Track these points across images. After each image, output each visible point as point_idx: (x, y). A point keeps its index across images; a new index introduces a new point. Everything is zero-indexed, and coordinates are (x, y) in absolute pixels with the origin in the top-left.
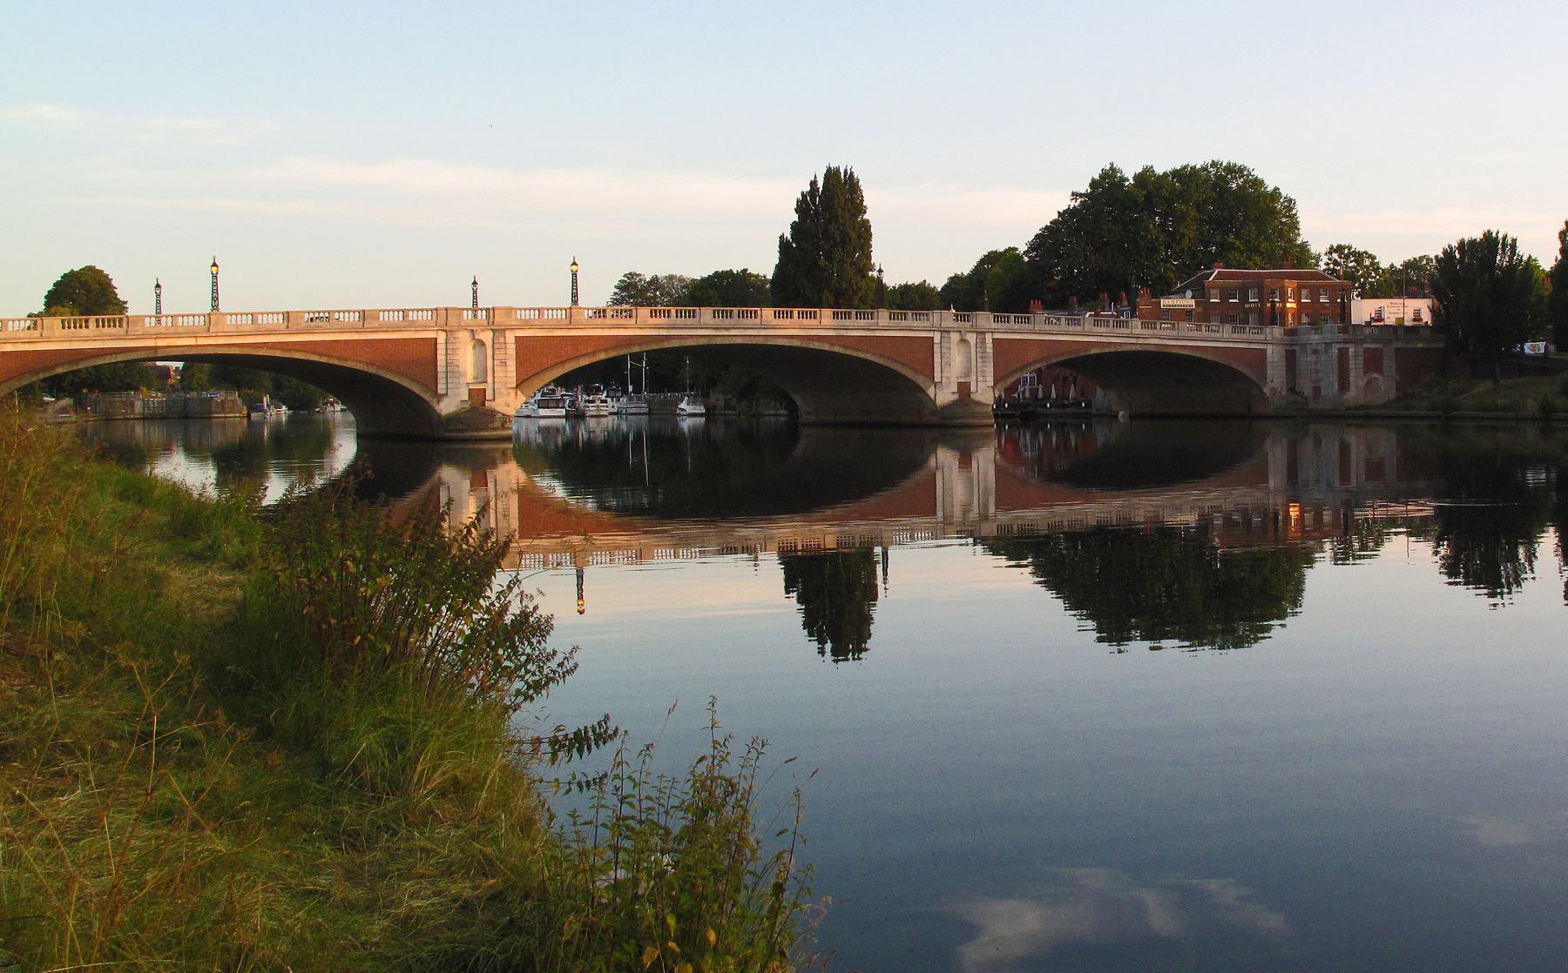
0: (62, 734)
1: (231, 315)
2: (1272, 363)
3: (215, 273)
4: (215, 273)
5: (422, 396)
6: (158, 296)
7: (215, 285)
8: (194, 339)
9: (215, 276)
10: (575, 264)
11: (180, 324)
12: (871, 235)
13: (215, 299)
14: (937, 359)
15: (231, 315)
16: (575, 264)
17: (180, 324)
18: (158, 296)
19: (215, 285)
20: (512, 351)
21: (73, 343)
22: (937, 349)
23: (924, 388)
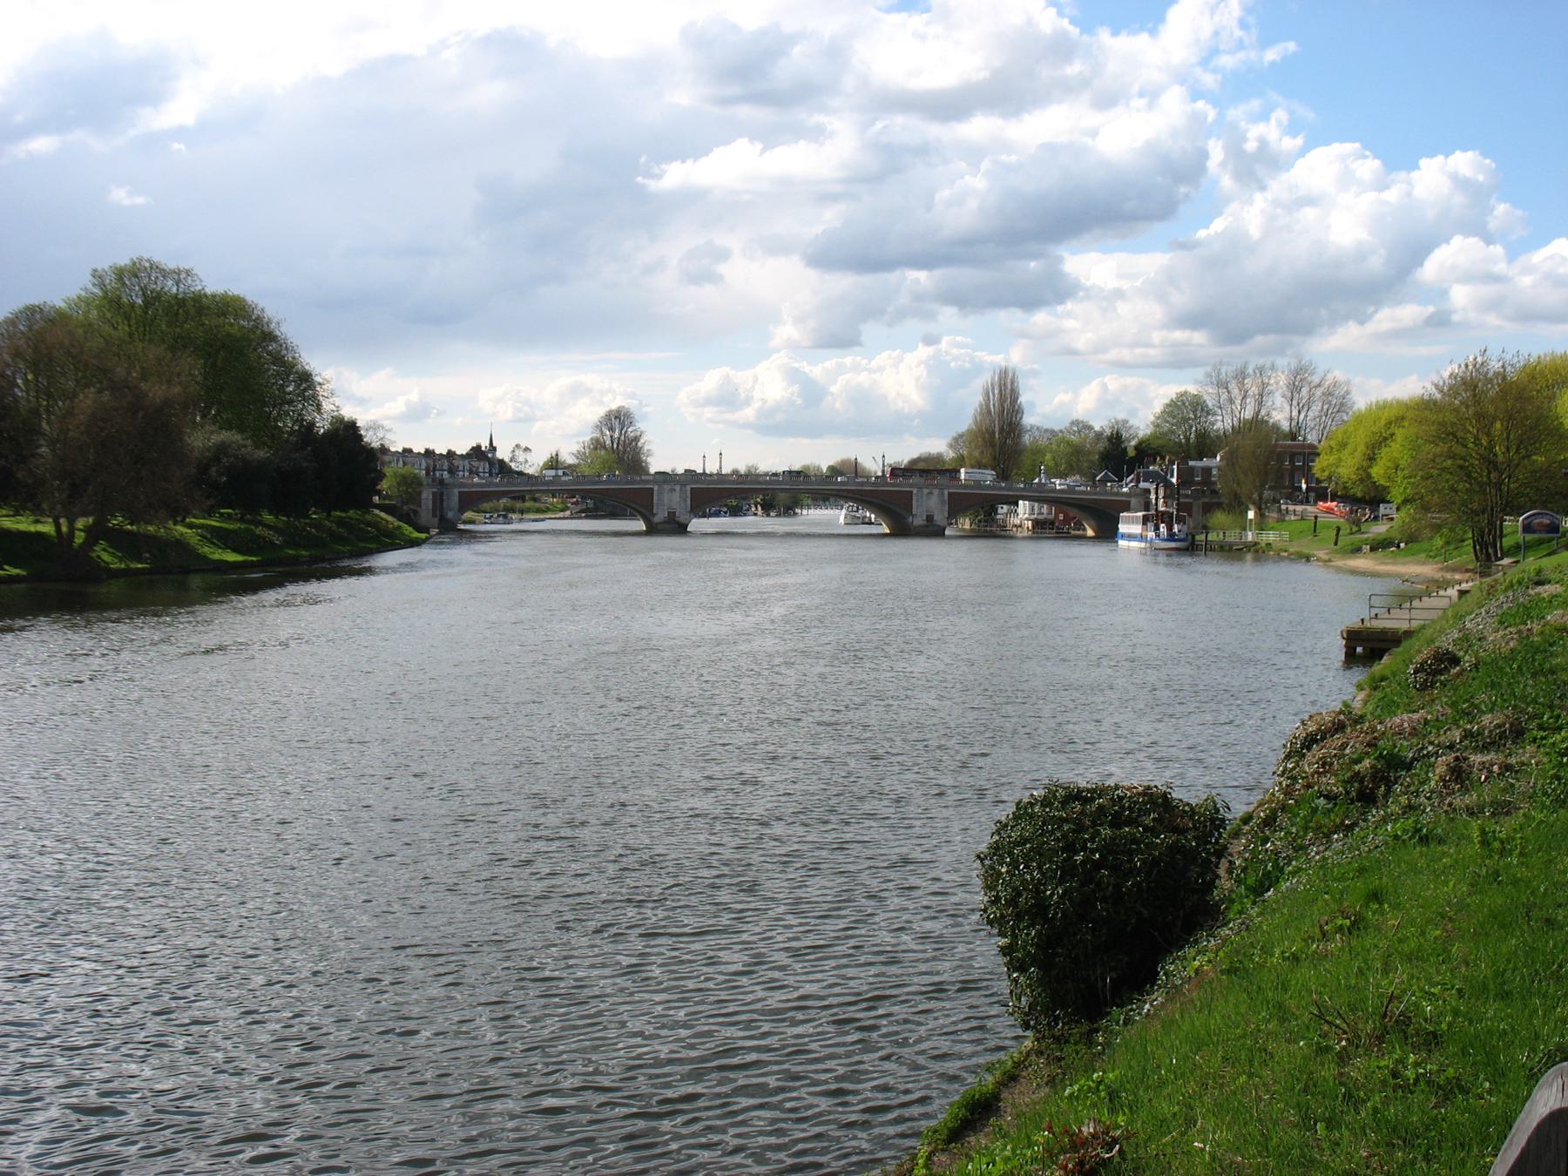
14: (914, 502)
20: (689, 493)
22: (914, 497)
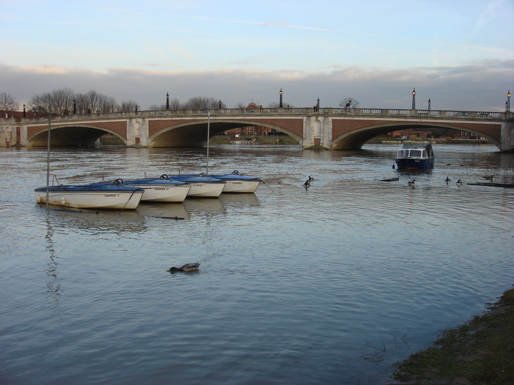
0: (50, 116)
1: (408, 110)
2: (504, 182)
3: (414, 94)
4: (414, 94)
5: (250, 124)
6: (429, 104)
7: (414, 99)
8: (303, 117)
9: (414, 96)
10: (281, 91)
11: (390, 113)
12: (175, 267)
13: (414, 104)
15: (408, 110)
16: (281, 91)
17: (390, 113)
18: (429, 104)
19: (414, 99)
21: (245, 117)
23: (23, 113)
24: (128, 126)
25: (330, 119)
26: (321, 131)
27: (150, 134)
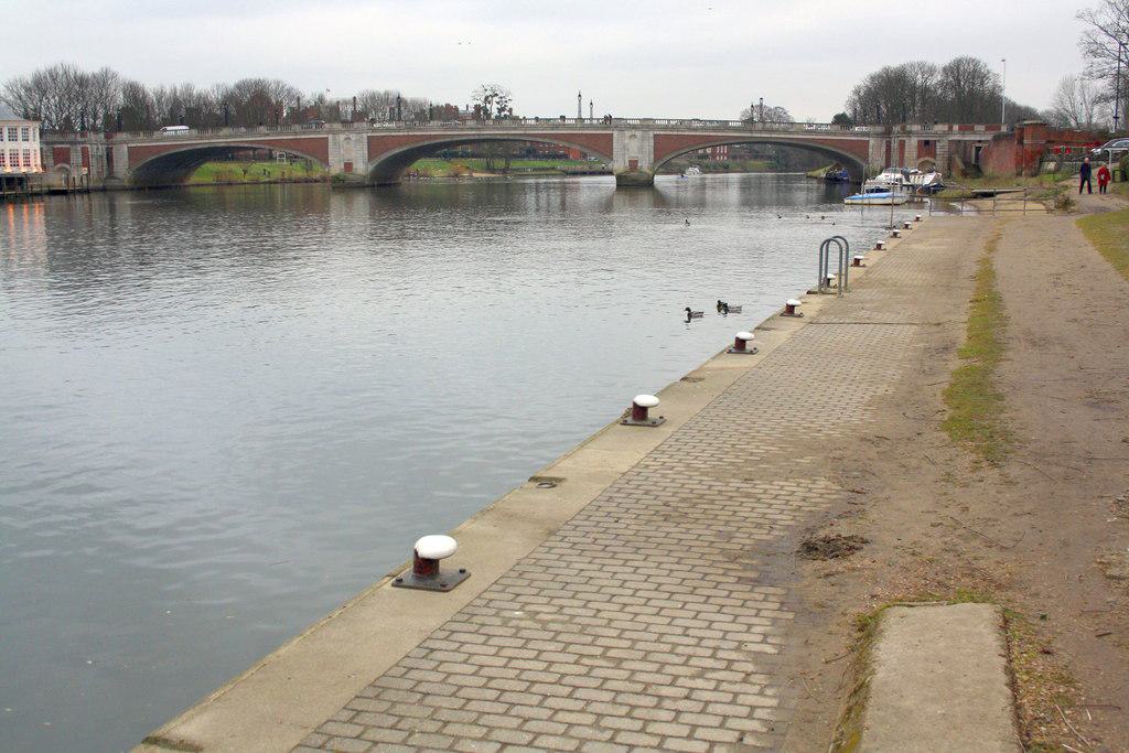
24: (330, 144)
25: (651, 134)
26: (641, 150)
27: (371, 157)
